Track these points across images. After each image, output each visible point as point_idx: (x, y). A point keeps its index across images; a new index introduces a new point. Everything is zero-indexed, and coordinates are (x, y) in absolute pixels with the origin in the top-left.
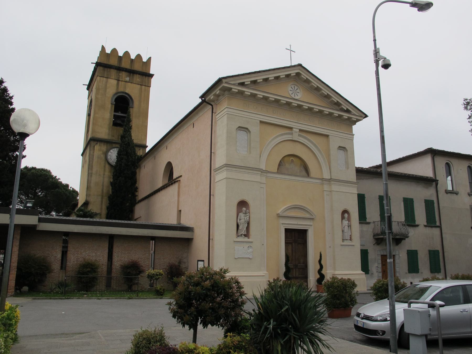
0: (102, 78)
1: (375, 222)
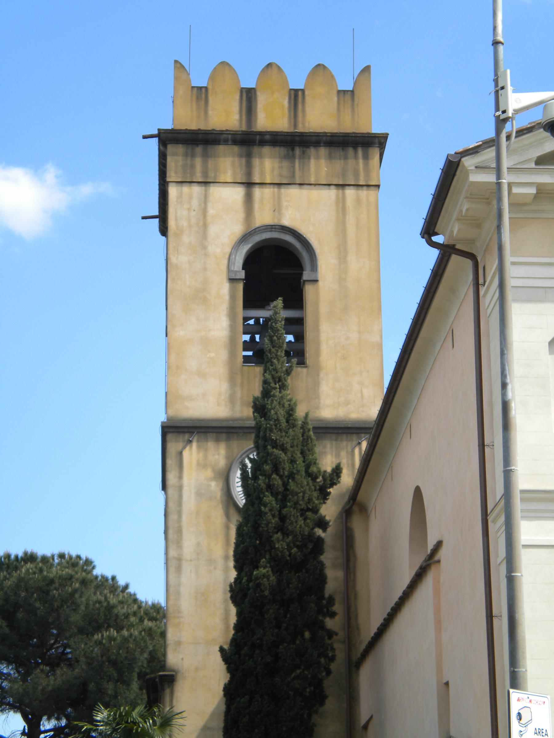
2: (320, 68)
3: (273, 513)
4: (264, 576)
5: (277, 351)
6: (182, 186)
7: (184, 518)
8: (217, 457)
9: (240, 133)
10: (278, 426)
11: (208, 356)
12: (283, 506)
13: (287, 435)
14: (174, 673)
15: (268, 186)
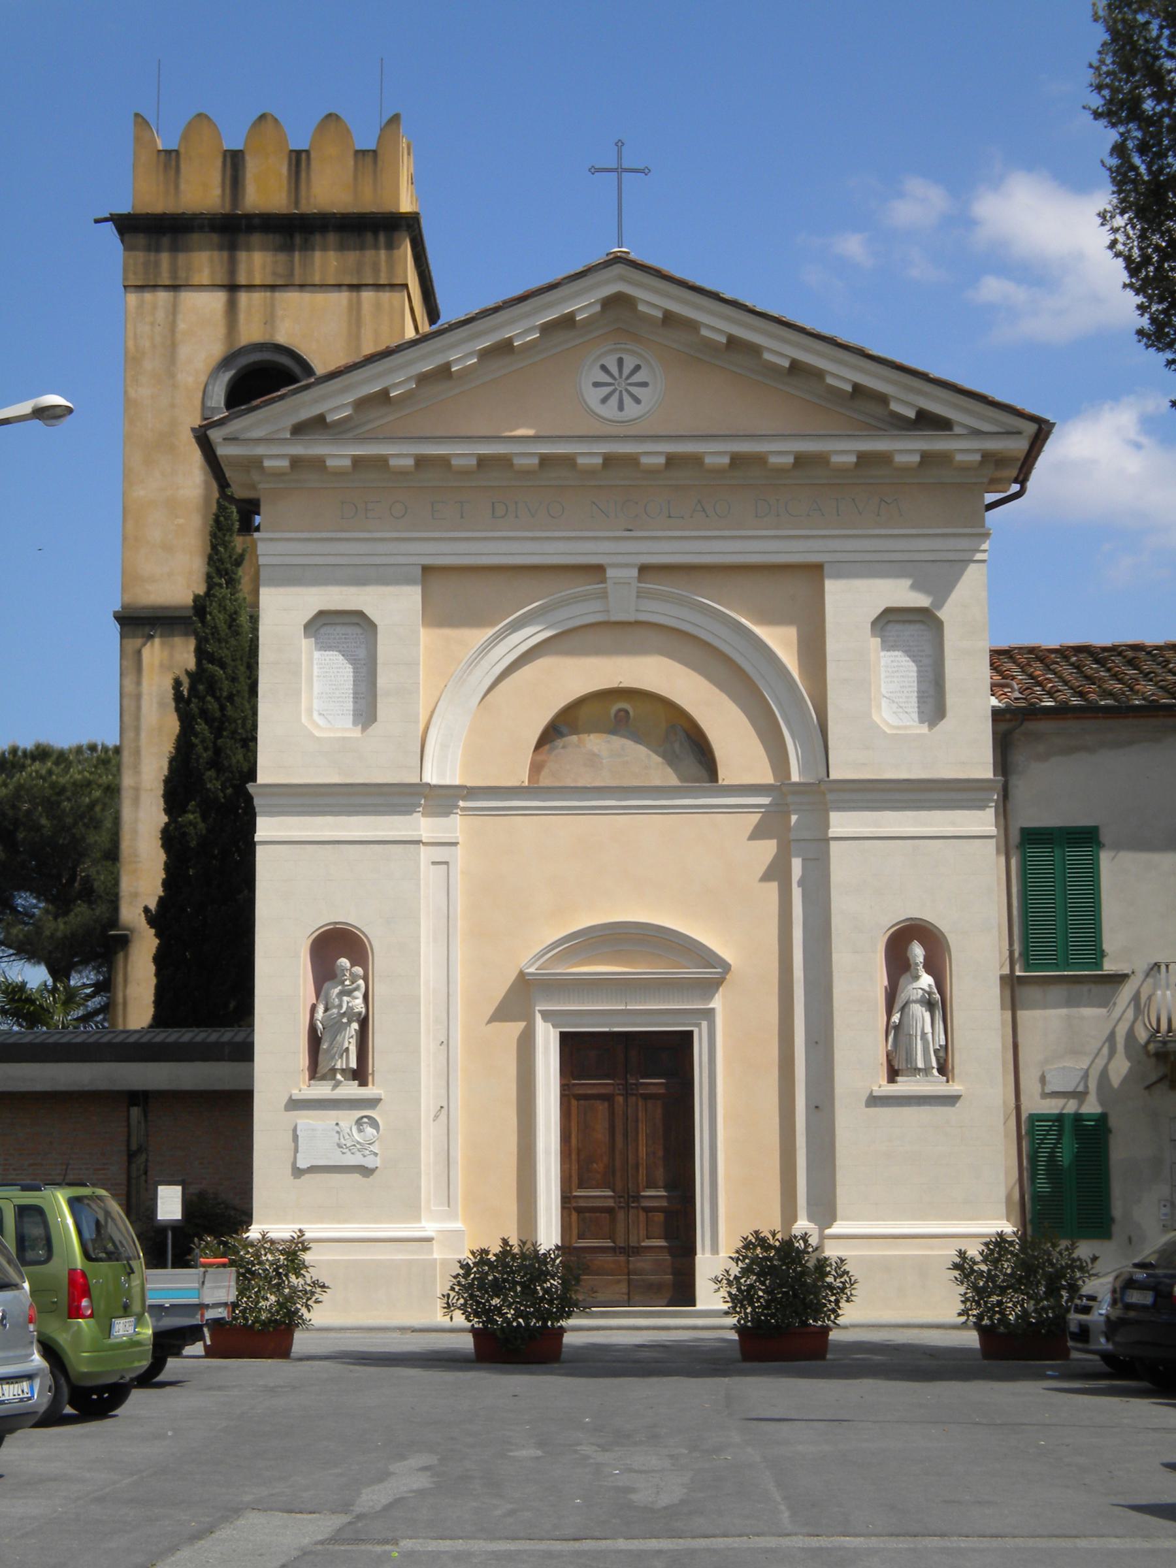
0: (148, 296)
1: (1163, 968)
2: (331, 118)
3: (205, 745)
4: (191, 823)
5: (224, 535)
6: (143, 292)
7: (143, 735)
8: (186, 655)
9: (220, 216)
10: (216, 634)
11: (176, 523)
12: (218, 735)
13: (228, 646)
14: (128, 932)
15: (258, 288)
